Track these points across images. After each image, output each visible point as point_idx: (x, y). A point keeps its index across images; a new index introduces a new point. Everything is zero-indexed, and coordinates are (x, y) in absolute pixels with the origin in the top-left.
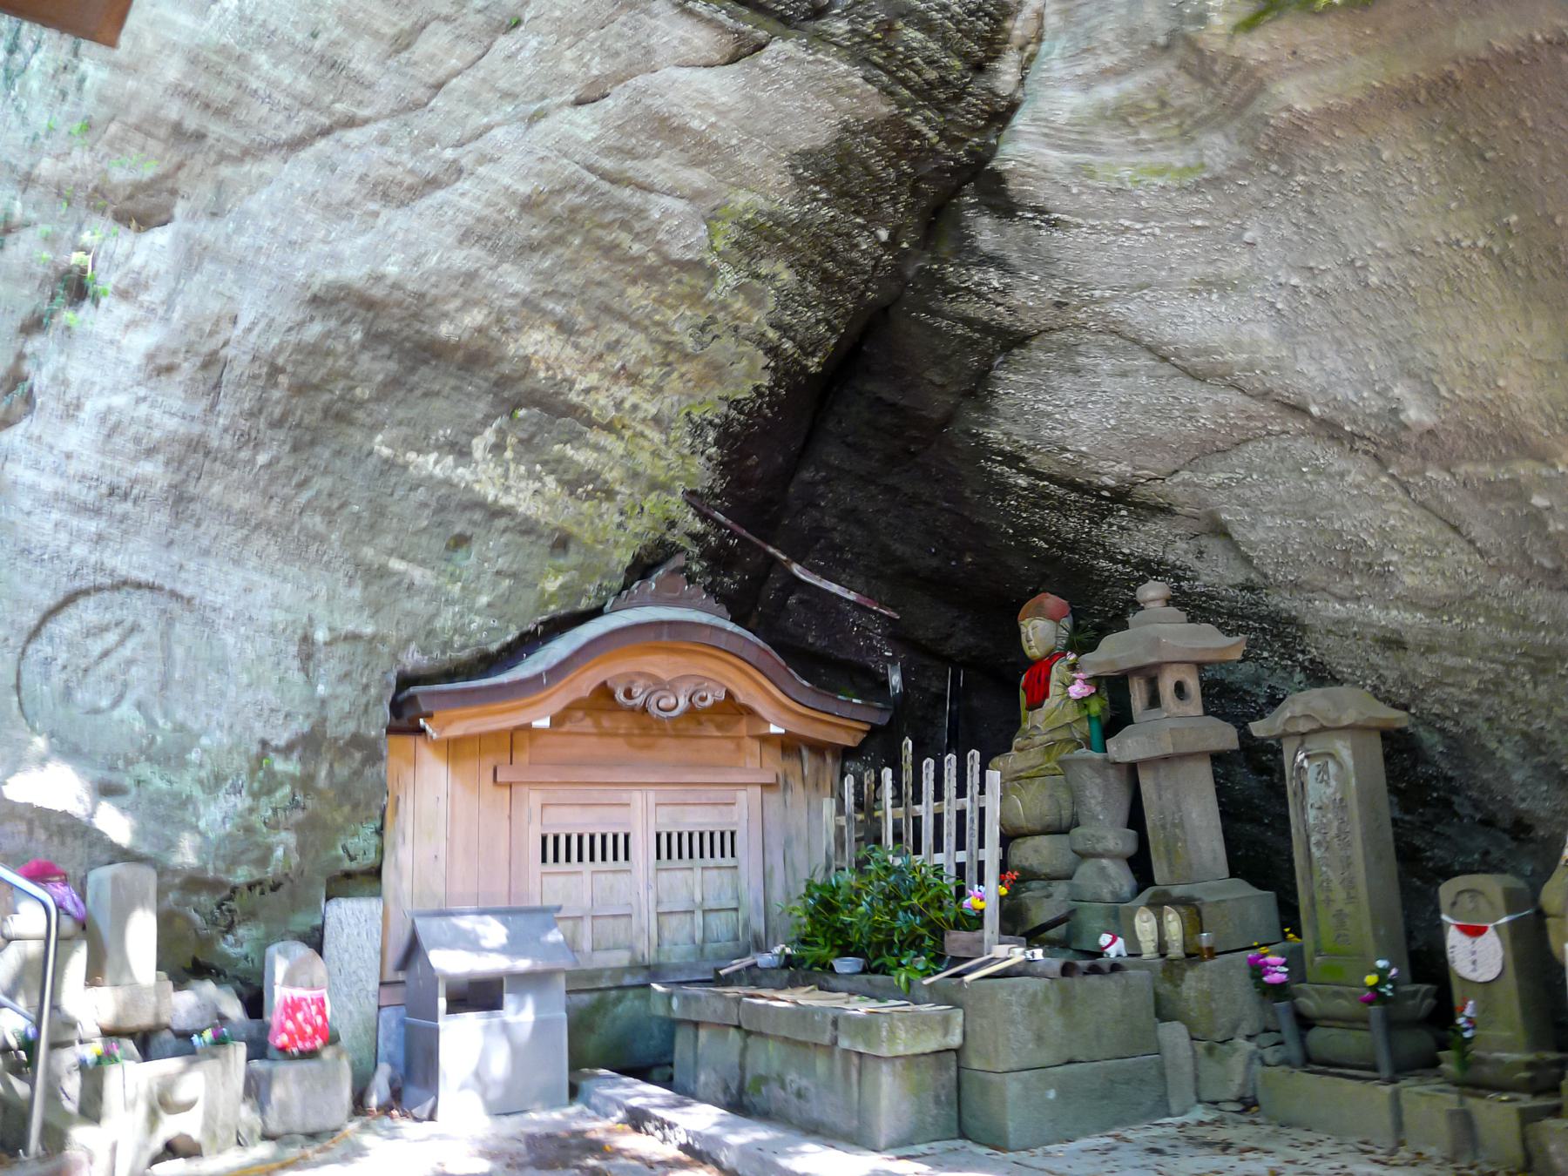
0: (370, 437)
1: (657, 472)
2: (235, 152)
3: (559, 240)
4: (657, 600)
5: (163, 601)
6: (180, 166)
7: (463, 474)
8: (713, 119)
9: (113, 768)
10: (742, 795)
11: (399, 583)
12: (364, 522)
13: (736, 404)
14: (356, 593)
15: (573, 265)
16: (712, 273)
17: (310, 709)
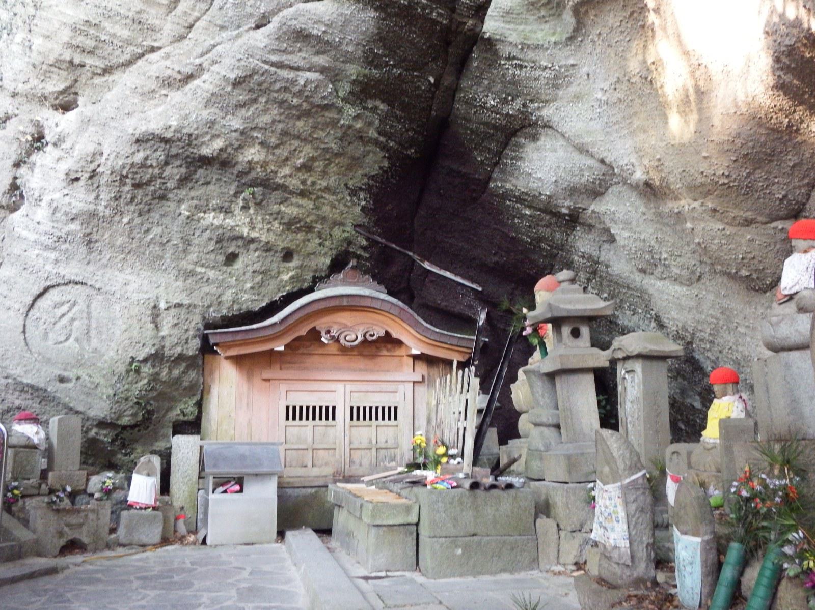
0: (179, 207)
1: (336, 216)
2: (99, 71)
3: (255, 101)
4: (345, 283)
5: (87, 290)
6: (76, 81)
7: (229, 222)
8: (324, 29)
9: (65, 370)
10: (401, 387)
11: (202, 278)
12: (180, 249)
13: (373, 177)
14: (180, 283)
15: (266, 111)
16: (340, 111)
17: (155, 342)
